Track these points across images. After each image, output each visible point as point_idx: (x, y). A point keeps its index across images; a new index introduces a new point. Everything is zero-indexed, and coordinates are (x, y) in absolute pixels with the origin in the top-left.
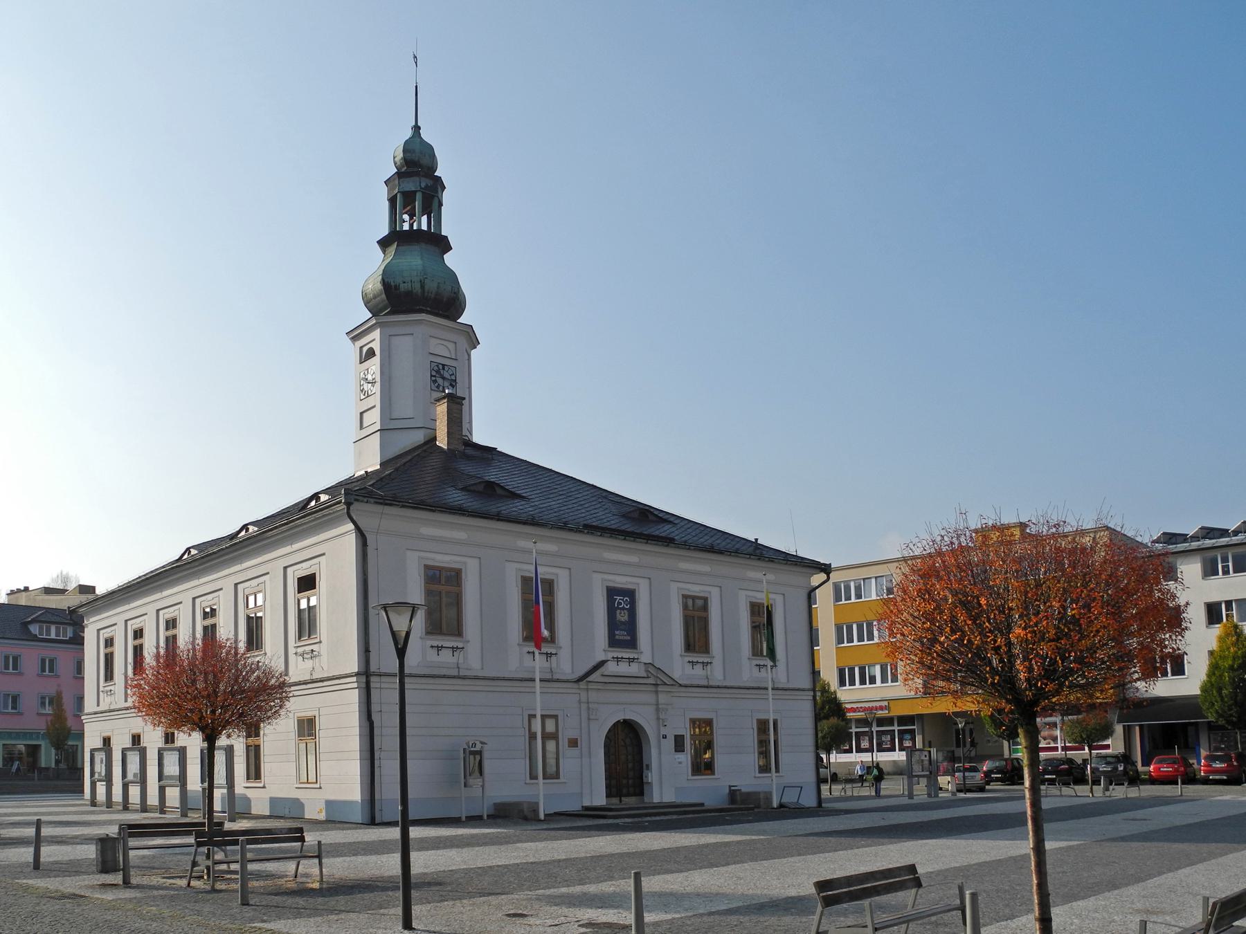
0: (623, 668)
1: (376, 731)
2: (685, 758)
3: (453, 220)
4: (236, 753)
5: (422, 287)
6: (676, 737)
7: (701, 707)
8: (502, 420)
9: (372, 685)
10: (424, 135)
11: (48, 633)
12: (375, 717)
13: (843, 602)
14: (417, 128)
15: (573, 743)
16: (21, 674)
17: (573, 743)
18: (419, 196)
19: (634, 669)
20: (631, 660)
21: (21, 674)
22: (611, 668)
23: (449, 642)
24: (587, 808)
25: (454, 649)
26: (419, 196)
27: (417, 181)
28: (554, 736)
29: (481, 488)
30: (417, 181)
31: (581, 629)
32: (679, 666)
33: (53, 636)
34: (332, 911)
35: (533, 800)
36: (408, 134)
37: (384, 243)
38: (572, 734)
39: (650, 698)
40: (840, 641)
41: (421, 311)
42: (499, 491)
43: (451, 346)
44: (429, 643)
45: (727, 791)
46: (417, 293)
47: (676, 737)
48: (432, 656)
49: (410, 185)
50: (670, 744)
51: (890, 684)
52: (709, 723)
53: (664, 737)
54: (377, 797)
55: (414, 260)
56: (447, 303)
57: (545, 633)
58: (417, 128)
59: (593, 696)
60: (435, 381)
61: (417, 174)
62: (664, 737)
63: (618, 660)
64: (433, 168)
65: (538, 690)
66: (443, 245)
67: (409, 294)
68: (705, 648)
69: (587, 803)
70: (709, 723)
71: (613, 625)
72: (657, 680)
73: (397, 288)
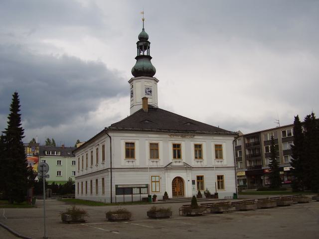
0: (178, 164)
3: (153, 51)
4: (115, 193)
7: (200, 173)
14: (143, 29)
19: (181, 164)
22: (174, 164)
23: (155, 160)
27: (143, 43)
30: (143, 43)
32: (194, 163)
34: (176, 136)
36: (140, 31)
37: (136, 58)
47: (127, 144)
48: (151, 164)
49: (141, 44)
50: (191, 182)
52: (133, 144)
57: (243, 191)
58: (143, 29)
64: (147, 39)
66: (149, 58)
67: (140, 71)
68: (221, 157)
70: (133, 144)
71: (221, 151)
72: (187, 167)
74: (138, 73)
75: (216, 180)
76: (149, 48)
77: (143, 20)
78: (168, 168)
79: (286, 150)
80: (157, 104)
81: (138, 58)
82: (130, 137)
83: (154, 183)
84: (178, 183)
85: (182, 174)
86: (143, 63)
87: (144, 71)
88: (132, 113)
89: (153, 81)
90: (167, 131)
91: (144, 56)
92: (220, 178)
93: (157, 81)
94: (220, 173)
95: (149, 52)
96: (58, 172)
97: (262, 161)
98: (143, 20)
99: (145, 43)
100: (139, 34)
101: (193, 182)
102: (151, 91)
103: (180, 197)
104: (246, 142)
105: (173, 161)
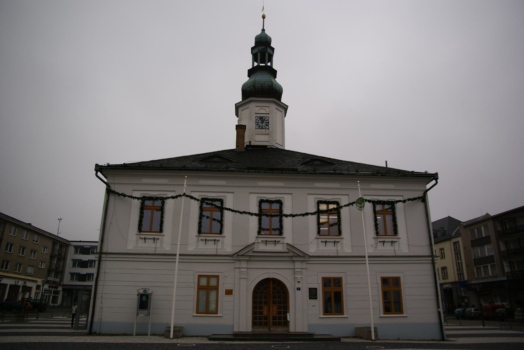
0: (270, 248)
2: (319, 302)
7: (332, 271)
9: (102, 259)
10: (266, 32)
14: (263, 30)
15: (229, 292)
17: (229, 292)
19: (279, 248)
22: (262, 247)
25: (392, 242)
27: (263, 49)
28: (216, 288)
30: (263, 49)
31: (240, 229)
32: (314, 246)
35: (368, 326)
36: (259, 32)
38: (229, 287)
39: (290, 265)
41: (273, 97)
43: (267, 109)
44: (320, 240)
46: (262, 89)
47: (310, 289)
53: (299, 289)
56: (274, 93)
58: (263, 30)
59: (244, 265)
60: (258, 124)
62: (299, 289)
65: (367, 262)
66: (274, 73)
72: (295, 255)
74: (250, 93)
77: (264, 17)
78: (245, 255)
79: (254, 318)
80: (283, 145)
81: (251, 73)
82: (211, 187)
83: (71, 322)
84: (270, 297)
85: (282, 273)
86: (262, 78)
89: (273, 107)
93: (285, 108)
94: (391, 271)
95: (272, 64)
96: (4, 261)
98: (264, 17)
99: (263, 47)
101: (313, 294)
102: (257, 124)
103: (279, 330)
104: (499, 229)
105: (260, 240)
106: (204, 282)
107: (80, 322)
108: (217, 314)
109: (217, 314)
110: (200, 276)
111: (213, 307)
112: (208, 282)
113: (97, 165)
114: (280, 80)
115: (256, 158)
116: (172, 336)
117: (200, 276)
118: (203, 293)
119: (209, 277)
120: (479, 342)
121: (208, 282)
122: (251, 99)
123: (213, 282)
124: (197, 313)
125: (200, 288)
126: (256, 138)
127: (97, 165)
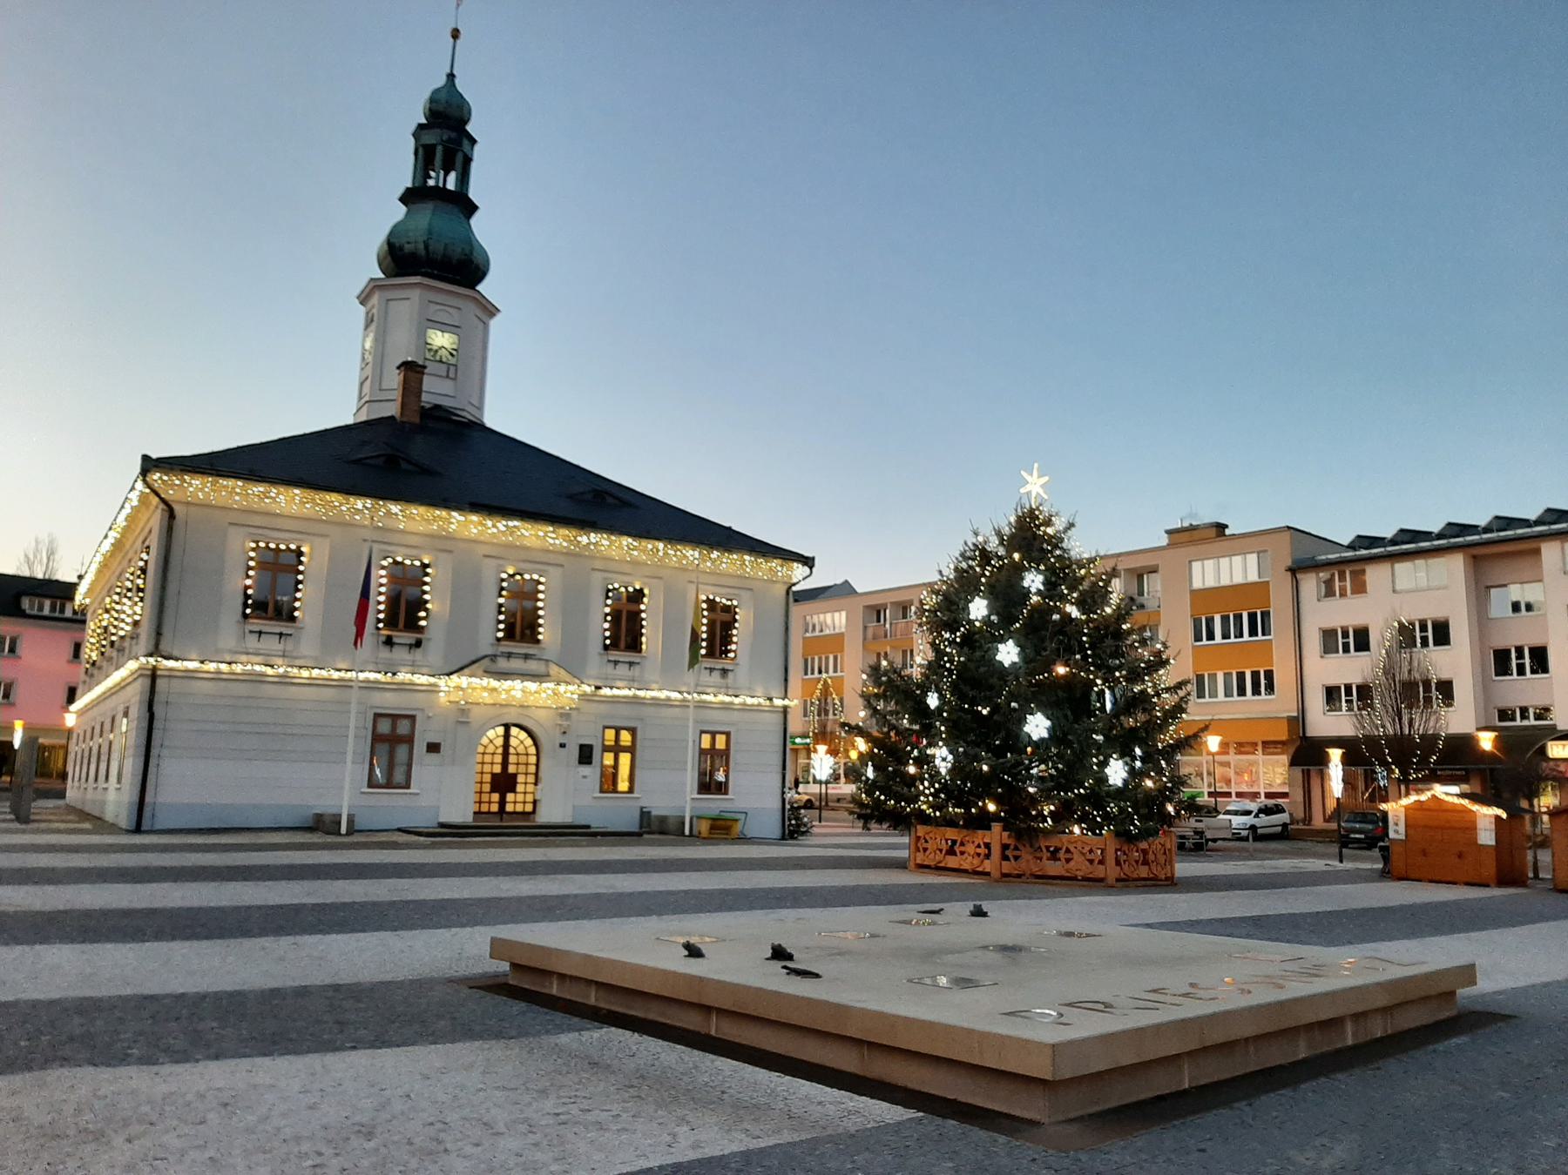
1: (156, 724)
5: (426, 247)
6: (582, 746)
8: (519, 403)
11: (41, 608)
12: (157, 709)
13: (1205, 642)
14: (451, 76)
15: (433, 748)
16: (13, 705)
17: (433, 748)
18: (439, 150)
20: (527, 657)
21: (13, 705)
24: (442, 825)
26: (439, 150)
27: (445, 133)
28: (409, 740)
29: (589, 497)
30: (445, 133)
33: (46, 611)
36: (441, 81)
40: (1198, 638)
42: (610, 500)
45: (637, 814)
47: (582, 746)
49: (429, 138)
51: (1236, 698)
53: (562, 746)
54: (148, 799)
55: (426, 214)
56: (464, 270)
58: (451, 76)
61: (439, 126)
62: (562, 746)
63: (509, 655)
64: (466, 122)
66: (471, 209)
67: (413, 255)
68: (634, 645)
69: (442, 820)
73: (401, 248)
74: (400, 260)
75: (1431, 613)
76: (468, 160)
77: (455, 34)
80: (480, 408)
81: (408, 197)
87: (435, 256)
88: (363, 417)
89: (471, 309)
90: (1101, 1007)
91: (440, 194)
92: (1329, 640)
93: (490, 310)
97: (1126, 884)
98: (455, 34)
99: (453, 135)
100: (427, 95)
106: (384, 727)
107: (1407, 732)
108: (408, 787)
109: (408, 787)
110: (377, 716)
111: (399, 776)
112: (394, 727)
113: (145, 458)
114: (481, 227)
115: (421, 447)
116: (687, 832)
117: (377, 716)
118: (383, 748)
119: (395, 718)
120: (124, 904)
121: (394, 727)
122: (417, 279)
123: (403, 728)
124: (370, 786)
125: (377, 738)
126: (434, 390)
127: (145, 458)
